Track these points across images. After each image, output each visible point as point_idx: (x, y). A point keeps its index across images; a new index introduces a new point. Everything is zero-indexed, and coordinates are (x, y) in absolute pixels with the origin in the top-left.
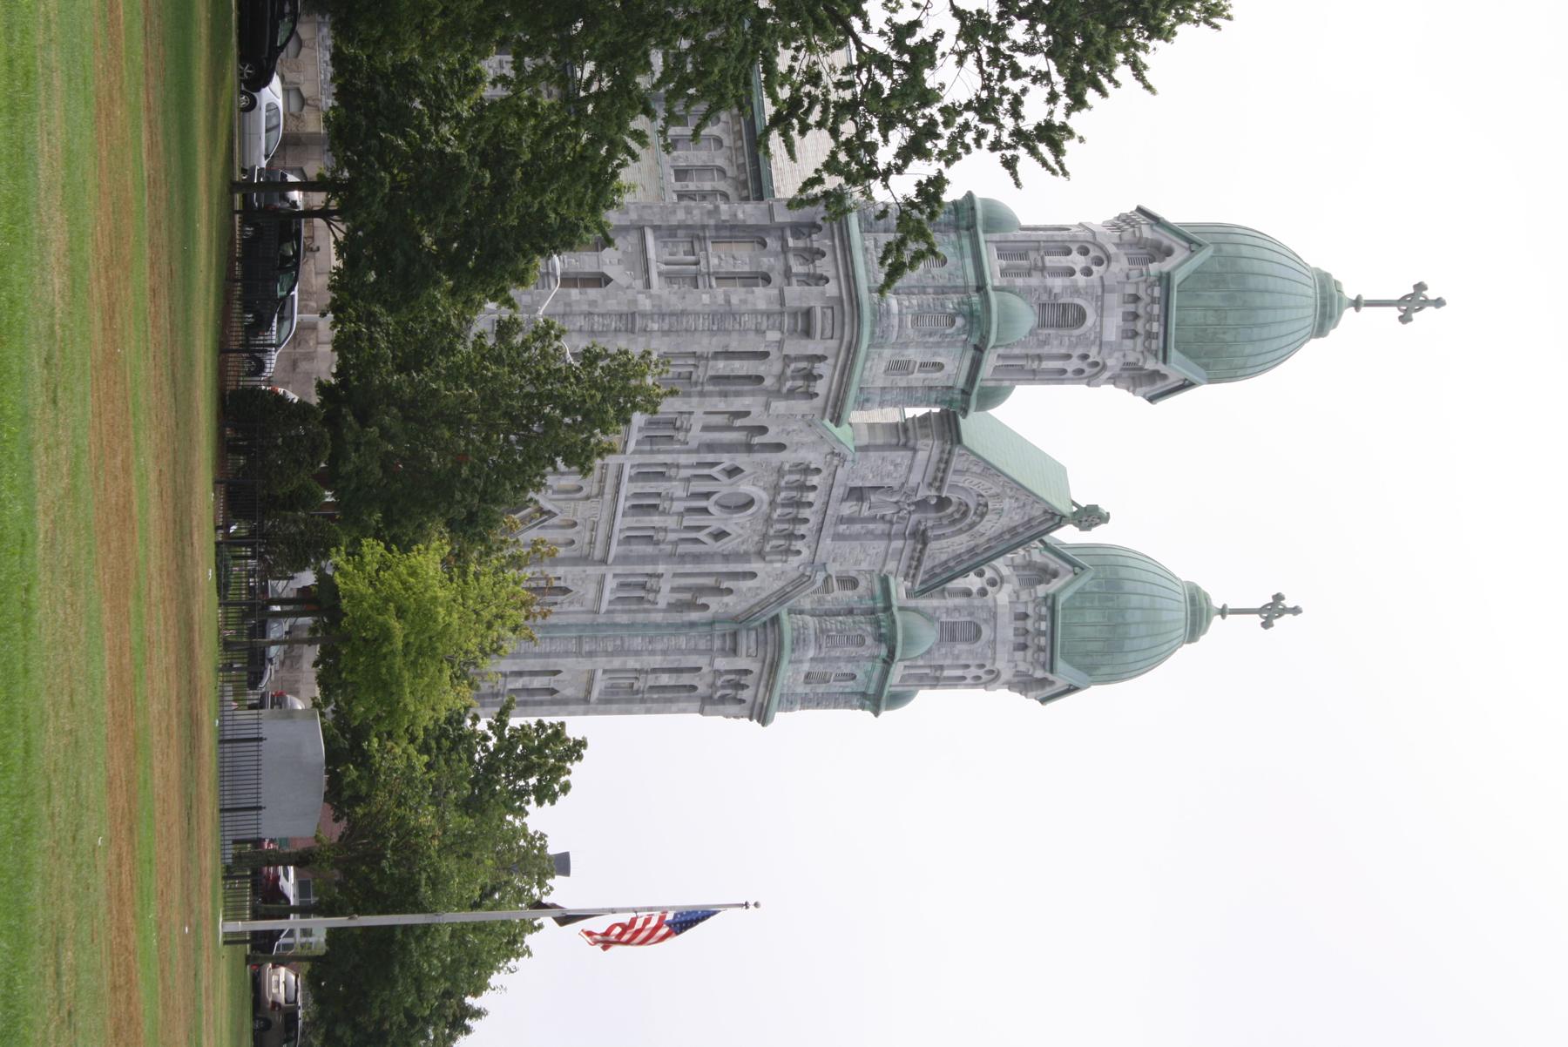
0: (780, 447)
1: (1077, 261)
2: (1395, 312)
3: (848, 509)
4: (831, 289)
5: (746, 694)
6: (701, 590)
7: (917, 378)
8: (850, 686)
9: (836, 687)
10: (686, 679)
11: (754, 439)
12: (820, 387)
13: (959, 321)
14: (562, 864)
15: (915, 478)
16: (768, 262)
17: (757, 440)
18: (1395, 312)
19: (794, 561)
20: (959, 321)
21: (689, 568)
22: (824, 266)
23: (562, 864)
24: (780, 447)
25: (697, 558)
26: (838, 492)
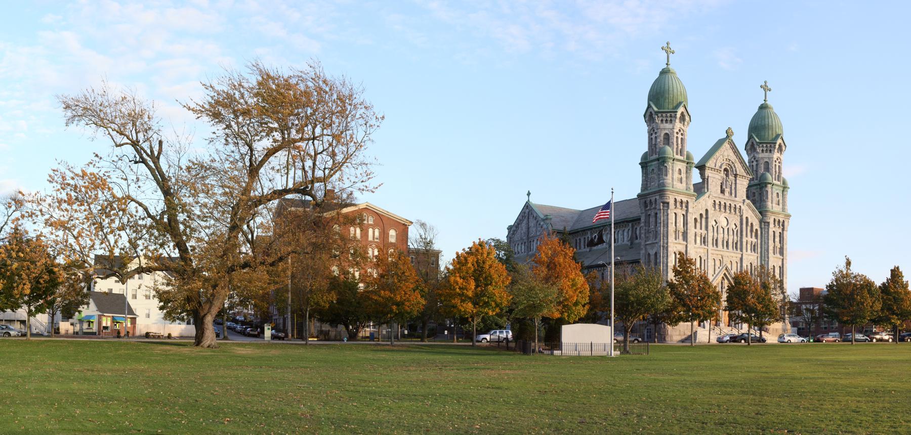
0: (707, 210)
1: (654, 136)
2: (768, 92)
3: (727, 194)
4: (657, 197)
5: (781, 220)
6: (752, 231)
7: (683, 175)
8: (780, 194)
9: (781, 198)
10: (777, 235)
11: (705, 216)
12: (685, 200)
13: (290, 125)
14: (457, 253)
15: (717, 176)
16: (653, 214)
17: (704, 216)
18: (768, 92)
19: (743, 207)
20: (290, 125)
21: (744, 233)
22: (653, 199)
23: (457, 253)
24: (707, 210)
25: (741, 231)
26: (721, 196)
